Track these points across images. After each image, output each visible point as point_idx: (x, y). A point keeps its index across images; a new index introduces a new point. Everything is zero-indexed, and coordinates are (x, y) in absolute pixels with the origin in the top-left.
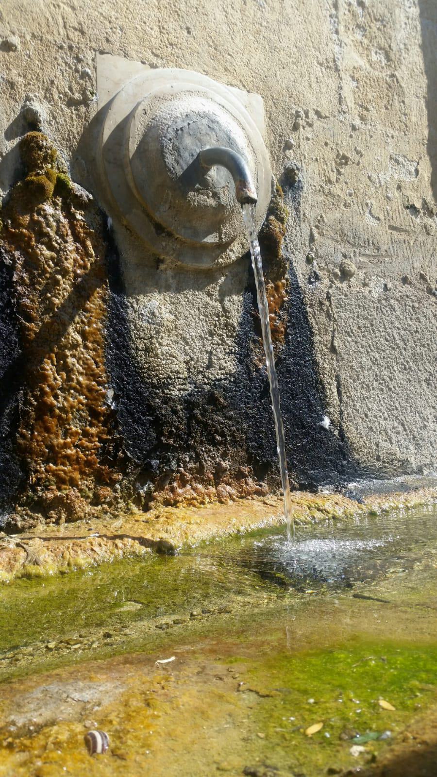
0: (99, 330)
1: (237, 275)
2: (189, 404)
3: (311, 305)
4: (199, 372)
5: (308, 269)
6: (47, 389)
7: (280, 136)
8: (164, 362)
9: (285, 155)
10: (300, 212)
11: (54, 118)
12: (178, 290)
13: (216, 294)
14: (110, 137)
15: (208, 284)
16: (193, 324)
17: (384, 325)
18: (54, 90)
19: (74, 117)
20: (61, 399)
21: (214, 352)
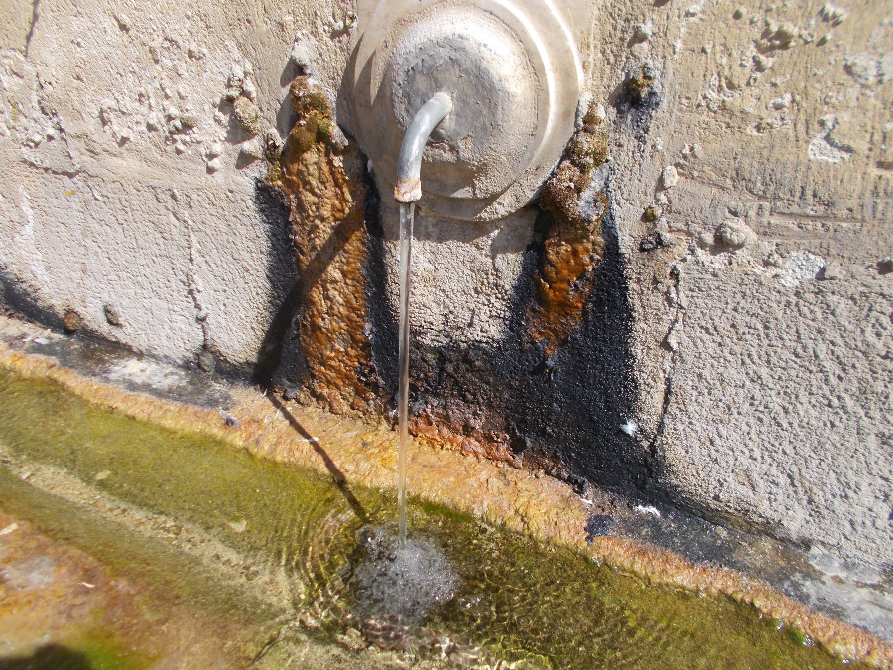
0: (358, 270)
1: (516, 229)
2: (441, 355)
3: (639, 280)
4: (459, 328)
5: (645, 230)
6: (315, 313)
7: (627, 21)
8: (417, 311)
9: (632, 54)
10: (645, 143)
11: (321, 55)
12: (440, 240)
13: (487, 249)
14: (361, 75)
15: (478, 236)
16: (456, 278)
17: (797, 331)
18: (319, 22)
19: (338, 50)
20: (327, 321)
21: (477, 311)
